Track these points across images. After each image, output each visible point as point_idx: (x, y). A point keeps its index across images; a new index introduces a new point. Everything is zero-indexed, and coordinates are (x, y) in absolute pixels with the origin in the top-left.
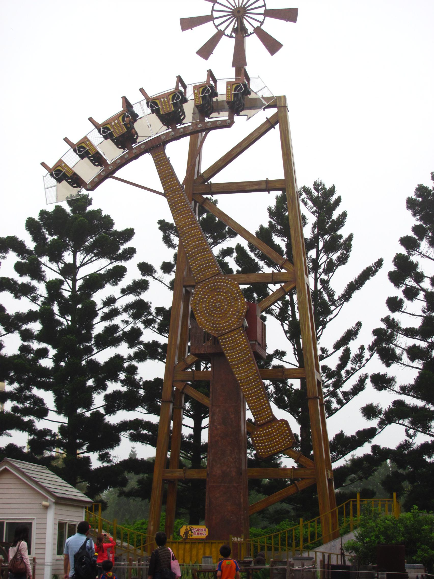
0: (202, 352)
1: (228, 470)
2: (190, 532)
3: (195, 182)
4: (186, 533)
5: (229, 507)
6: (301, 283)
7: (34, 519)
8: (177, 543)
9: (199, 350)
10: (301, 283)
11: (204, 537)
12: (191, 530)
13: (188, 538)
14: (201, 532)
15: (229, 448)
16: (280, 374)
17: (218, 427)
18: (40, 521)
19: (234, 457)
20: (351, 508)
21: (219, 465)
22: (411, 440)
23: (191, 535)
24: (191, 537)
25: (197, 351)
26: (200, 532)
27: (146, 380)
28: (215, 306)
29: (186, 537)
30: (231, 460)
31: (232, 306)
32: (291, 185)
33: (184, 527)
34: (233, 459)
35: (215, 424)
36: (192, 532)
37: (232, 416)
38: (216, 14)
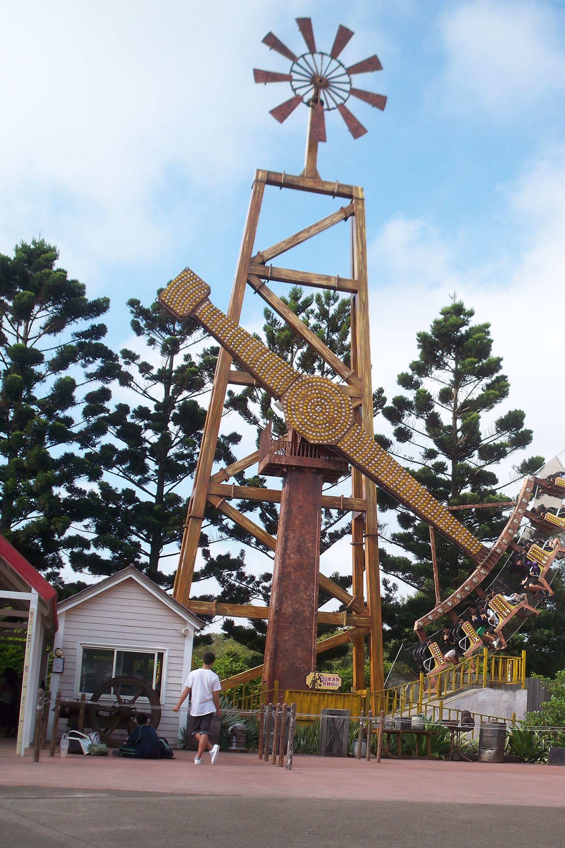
0: (283, 463)
1: (301, 608)
2: (319, 681)
3: (252, 261)
4: (314, 682)
5: (299, 654)
6: (367, 401)
7: (165, 650)
8: (318, 695)
9: (279, 460)
10: (367, 401)
11: (336, 688)
12: (320, 678)
13: (316, 688)
14: (333, 682)
15: (304, 582)
16: (337, 503)
17: (292, 556)
18: (173, 654)
19: (308, 593)
20: (493, 665)
21: (290, 602)
22: (391, 595)
23: (320, 685)
24: (319, 688)
25: (277, 460)
26: (331, 682)
27: (413, 470)
28: (321, 406)
29: (314, 686)
30: (305, 596)
31: (302, 413)
32: (364, 288)
33: (312, 675)
34: (307, 596)
35: (288, 552)
36: (321, 682)
37: (309, 545)
38: (301, 61)
